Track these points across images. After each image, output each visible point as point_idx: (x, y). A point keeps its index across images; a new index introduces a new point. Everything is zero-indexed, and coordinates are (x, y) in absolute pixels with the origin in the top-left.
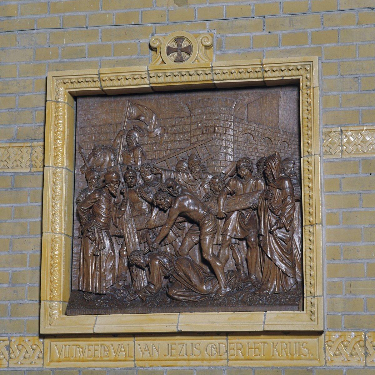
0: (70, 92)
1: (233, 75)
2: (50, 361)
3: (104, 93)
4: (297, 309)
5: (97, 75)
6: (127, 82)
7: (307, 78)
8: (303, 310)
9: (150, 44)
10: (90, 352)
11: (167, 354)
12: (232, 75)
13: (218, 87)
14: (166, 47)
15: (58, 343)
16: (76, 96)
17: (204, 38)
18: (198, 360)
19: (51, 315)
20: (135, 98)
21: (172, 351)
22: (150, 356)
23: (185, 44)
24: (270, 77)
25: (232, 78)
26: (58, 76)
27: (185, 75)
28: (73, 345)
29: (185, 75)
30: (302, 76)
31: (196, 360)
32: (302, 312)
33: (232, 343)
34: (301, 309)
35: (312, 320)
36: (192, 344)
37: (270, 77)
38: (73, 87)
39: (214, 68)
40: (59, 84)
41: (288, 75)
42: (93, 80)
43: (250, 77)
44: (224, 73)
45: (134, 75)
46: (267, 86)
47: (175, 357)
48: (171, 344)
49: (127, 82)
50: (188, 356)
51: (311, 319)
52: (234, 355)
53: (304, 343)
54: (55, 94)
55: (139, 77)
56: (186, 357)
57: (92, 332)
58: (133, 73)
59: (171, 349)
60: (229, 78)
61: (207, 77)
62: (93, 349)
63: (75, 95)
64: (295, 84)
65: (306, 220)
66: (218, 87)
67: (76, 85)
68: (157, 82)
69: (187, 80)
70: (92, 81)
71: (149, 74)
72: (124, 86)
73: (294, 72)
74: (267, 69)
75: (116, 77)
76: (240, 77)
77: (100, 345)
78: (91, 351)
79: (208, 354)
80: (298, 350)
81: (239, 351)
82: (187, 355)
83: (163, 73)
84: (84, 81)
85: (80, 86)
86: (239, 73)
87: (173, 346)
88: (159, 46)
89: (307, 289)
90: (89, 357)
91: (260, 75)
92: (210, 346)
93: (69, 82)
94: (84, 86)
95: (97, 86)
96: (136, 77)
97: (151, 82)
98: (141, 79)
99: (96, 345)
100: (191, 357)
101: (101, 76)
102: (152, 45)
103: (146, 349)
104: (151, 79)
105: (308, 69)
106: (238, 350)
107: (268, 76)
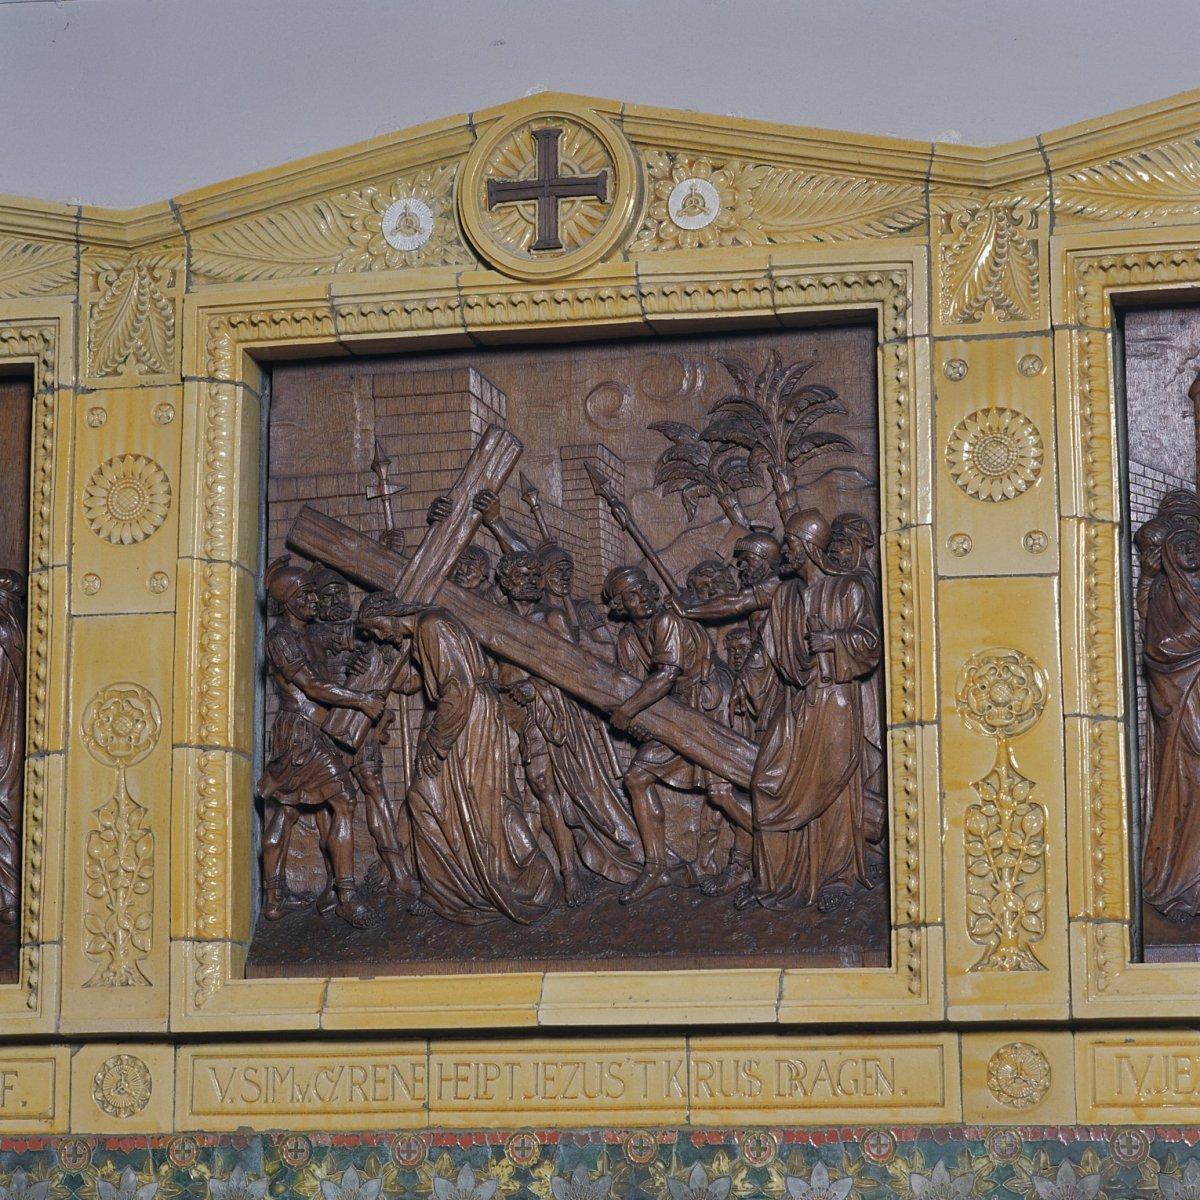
0: (249, 352)
2: (1094, 1106)
11: (533, 1093)
12: (665, 299)
13: (356, 352)
16: (269, 363)
22: (712, 1095)
24: (700, 311)
26: (852, 264)
28: (638, 1062)
30: (882, 301)
33: (383, 1066)
36: (737, 1062)
38: (256, 336)
39: (336, 302)
41: (855, 300)
44: (363, 314)
49: (801, 296)
54: (205, 358)
55: (591, 294)
56: (583, 1101)
57: (535, 1024)
58: (1147, 249)
64: (867, 320)
65: (895, 711)
69: (549, 317)
70: (794, 286)
71: (639, 286)
73: (859, 292)
74: (783, 283)
81: (357, 1089)
83: (310, 308)
84: (504, 300)
87: (551, 1070)
91: (766, 298)
98: (553, 303)
99: (11, 1072)
100: (596, 1102)
101: (642, 280)
103: (823, 1073)
105: (48, 336)
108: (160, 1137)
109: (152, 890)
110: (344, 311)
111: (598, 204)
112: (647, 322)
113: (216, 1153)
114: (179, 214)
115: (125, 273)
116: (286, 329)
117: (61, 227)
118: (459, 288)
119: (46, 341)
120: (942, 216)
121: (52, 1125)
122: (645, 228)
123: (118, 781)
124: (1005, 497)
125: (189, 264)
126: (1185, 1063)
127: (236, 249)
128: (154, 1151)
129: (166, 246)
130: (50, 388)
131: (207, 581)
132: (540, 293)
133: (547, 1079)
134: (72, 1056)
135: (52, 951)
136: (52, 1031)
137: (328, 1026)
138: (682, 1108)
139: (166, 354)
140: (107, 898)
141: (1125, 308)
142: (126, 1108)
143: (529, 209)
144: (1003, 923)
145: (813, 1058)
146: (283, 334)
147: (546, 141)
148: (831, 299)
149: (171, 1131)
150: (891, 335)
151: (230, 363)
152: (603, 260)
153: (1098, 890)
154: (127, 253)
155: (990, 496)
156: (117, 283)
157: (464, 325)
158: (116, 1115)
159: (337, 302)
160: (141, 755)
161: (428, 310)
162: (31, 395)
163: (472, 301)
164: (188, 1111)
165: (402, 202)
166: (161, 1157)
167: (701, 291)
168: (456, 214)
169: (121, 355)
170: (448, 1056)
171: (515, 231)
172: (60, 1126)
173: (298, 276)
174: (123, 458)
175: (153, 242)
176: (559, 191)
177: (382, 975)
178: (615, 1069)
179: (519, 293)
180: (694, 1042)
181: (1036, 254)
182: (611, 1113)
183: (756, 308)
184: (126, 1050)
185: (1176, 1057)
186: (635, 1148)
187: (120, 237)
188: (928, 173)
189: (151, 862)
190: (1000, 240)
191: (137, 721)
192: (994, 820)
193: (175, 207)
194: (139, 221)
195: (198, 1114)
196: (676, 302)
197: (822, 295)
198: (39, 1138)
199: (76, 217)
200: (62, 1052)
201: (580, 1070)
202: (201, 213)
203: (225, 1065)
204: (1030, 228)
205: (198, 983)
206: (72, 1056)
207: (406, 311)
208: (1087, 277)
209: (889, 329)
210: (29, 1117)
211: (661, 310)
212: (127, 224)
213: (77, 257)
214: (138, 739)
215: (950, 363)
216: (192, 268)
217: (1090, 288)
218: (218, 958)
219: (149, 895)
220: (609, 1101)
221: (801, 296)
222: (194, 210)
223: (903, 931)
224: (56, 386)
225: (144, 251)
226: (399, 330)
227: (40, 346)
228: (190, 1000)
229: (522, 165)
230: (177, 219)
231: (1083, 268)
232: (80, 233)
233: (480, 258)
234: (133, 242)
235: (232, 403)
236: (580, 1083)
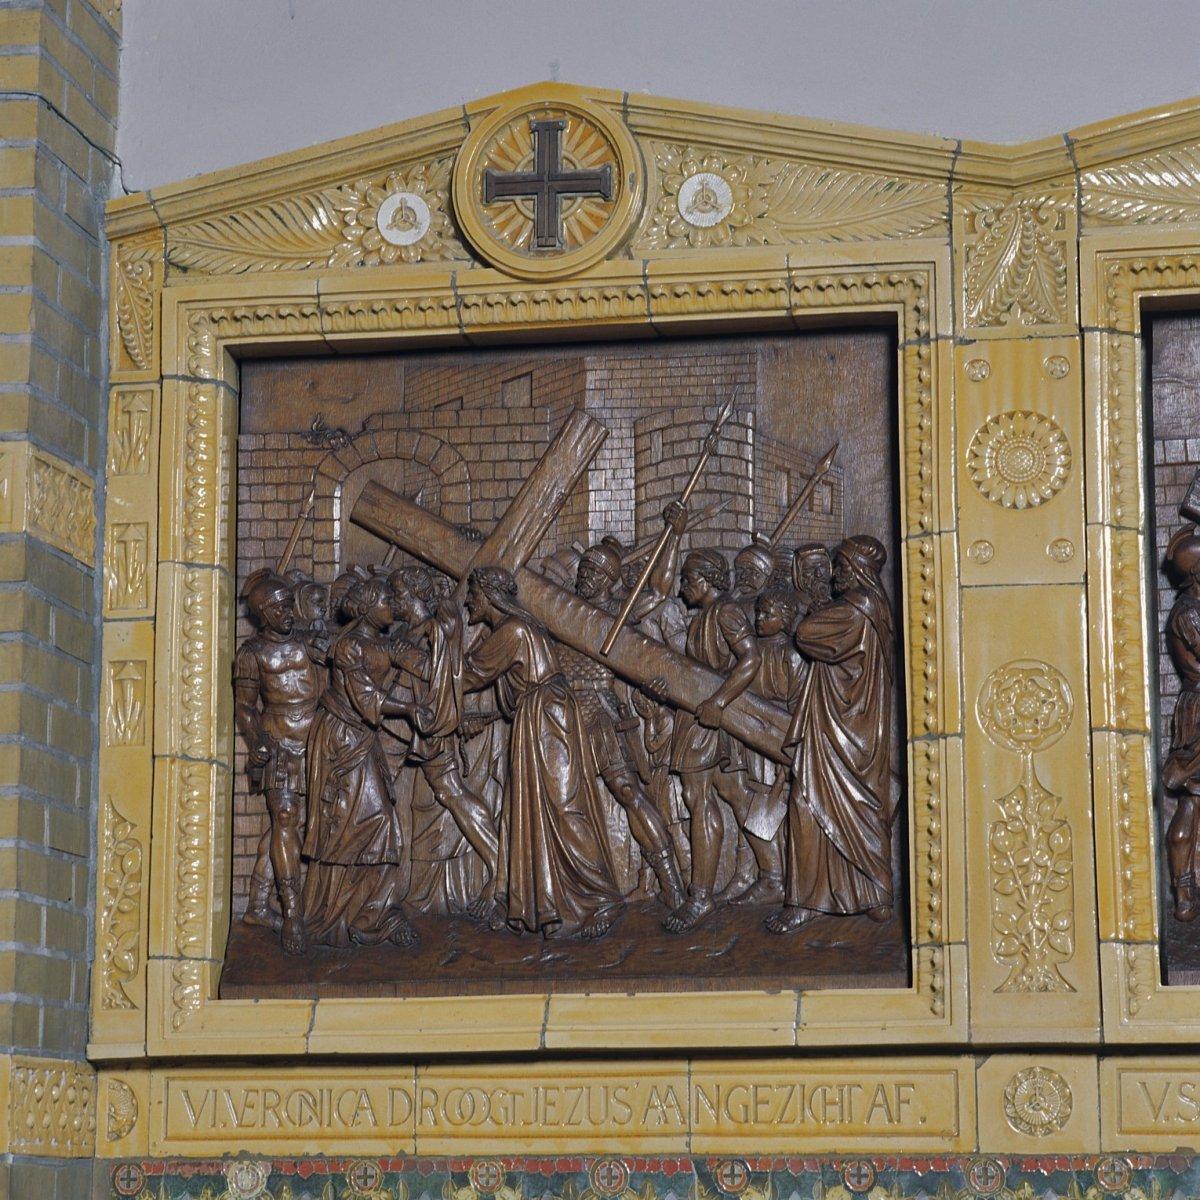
0: (227, 348)
5: (313, 296)
7: (917, 309)
8: (910, 985)
10: (906, 1105)
11: (532, 1119)
15: (233, 1085)
16: (244, 358)
21: (828, 1107)
24: (435, 327)
25: (376, 326)
30: (903, 302)
32: (907, 991)
34: (904, 981)
35: (934, 1012)
37: (411, 328)
39: (460, 292)
40: (197, 324)
42: (277, 311)
47: (553, 1128)
48: (546, 1089)
55: (737, 287)
62: (261, 1101)
64: (884, 326)
70: (274, 316)
73: (881, 293)
74: (658, 291)
75: (414, 303)
78: (908, 1102)
79: (815, 1118)
85: (725, 306)
89: (921, 923)
91: (783, 299)
92: (296, 1097)
94: (275, 329)
95: (312, 329)
96: (752, 286)
100: (603, 1128)
101: (322, 298)
104: (653, 301)
105: (920, 281)
108: (1085, 1157)
109: (1071, 887)
110: (331, 309)
111: (601, 201)
112: (793, 318)
113: (1152, 1176)
114: (1072, 150)
115: (1006, 214)
117: (933, 163)
119: (917, 286)
120: (966, 216)
121: (957, 1143)
122: (655, 224)
123: (1025, 767)
124: (1030, 505)
125: (1079, 206)
126: (906, 1092)
127: (204, 238)
128: (1079, 1173)
129: (1053, 185)
130: (924, 339)
132: (541, 292)
133: (900, 1102)
134: (977, 1068)
135: (958, 951)
136: (964, 1039)
137: (804, 1042)
138: (681, 1135)
139: (1057, 303)
140: (1017, 897)
141: (1155, 314)
142: (1042, 1125)
143: (526, 206)
144: (1030, 942)
145: (338, 1085)
146: (1189, 282)
147: (547, 133)
148: (827, 302)
149: (1097, 1152)
151: (211, 363)
152: (609, 257)
153: (1129, 912)
154: (1008, 192)
155: (1000, 500)
156: (997, 224)
157: (459, 326)
158: (1031, 1134)
160: (1052, 738)
163: (469, 301)
164: (163, 1136)
165: (398, 197)
166: (1089, 1180)
168: (451, 210)
169: (1003, 304)
170: (888, 1077)
171: (513, 226)
172: (966, 1145)
173: (289, 269)
174: (1011, 416)
175: (1039, 180)
176: (557, 185)
177: (328, 997)
178: (621, 1093)
179: (519, 292)
180: (422, 1070)
181: (1064, 256)
182: (495, 1142)
183: (843, 305)
184: (1040, 1062)
185: (898, 1086)
186: (853, 1175)
187: (1004, 175)
188: (951, 172)
189: (1069, 854)
190: (1026, 241)
191: (1044, 702)
192: (1020, 838)
193: (1070, 143)
194: (1027, 157)
195: (1128, 1132)
197: (393, 319)
198: (940, 1159)
199: (953, 152)
200: (967, 1062)
201: (584, 1099)
202: (1099, 149)
203: (1156, 1080)
204: (1057, 228)
205: (175, 1003)
206: (977, 1068)
208: (1117, 280)
210: (931, 1134)
211: (668, 312)
212: (1013, 160)
213: (949, 196)
214: (1047, 723)
215: (1051, 359)
216: (1083, 209)
217: (1120, 291)
219: (1069, 890)
220: (616, 1127)
221: (820, 298)
222: (1090, 146)
223: (925, 951)
224: (932, 336)
225: (1028, 190)
226: (364, 331)
227: (906, 292)
228: (168, 1020)
229: (520, 157)
230: (1071, 155)
231: (1114, 269)
232: (957, 168)
233: (476, 256)
234: (1017, 180)
235: (213, 404)
236: (585, 1107)
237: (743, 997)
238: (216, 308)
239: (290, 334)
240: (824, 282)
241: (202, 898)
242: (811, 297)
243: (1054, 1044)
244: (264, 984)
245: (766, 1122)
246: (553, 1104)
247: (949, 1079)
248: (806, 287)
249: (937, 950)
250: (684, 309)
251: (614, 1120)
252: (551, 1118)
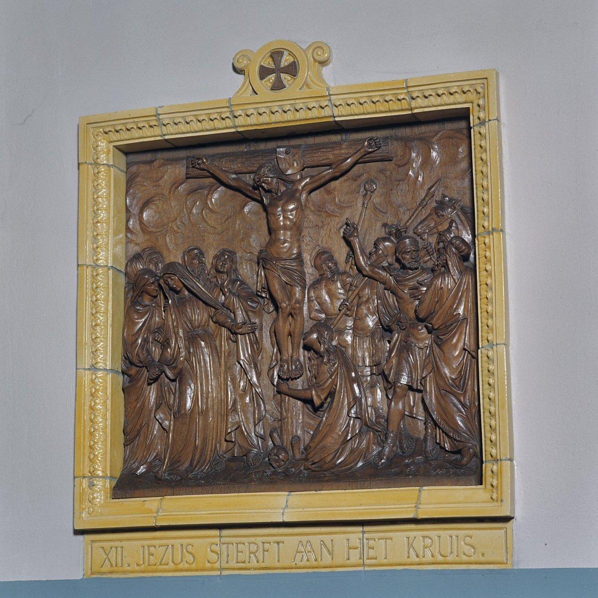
0: (117, 148)
1: (363, 107)
3: (168, 145)
4: (302, 489)
6: (439, 100)
7: (479, 106)
9: (235, 65)
12: (386, 103)
13: (247, 136)
14: (257, 69)
17: (316, 50)
18: (484, 564)
19: (91, 499)
20: (366, 134)
23: (286, 60)
24: (381, 112)
27: (288, 110)
29: (290, 110)
30: (472, 102)
31: (313, 568)
32: (480, 486)
33: (267, 543)
35: (493, 499)
37: (381, 112)
39: (410, 89)
40: (97, 135)
42: (220, 116)
43: (391, 109)
44: (348, 105)
45: (436, 88)
46: (420, 121)
49: (439, 100)
50: (444, 556)
51: (491, 498)
52: (244, 562)
53: (188, 545)
59: (238, 552)
60: (356, 111)
61: (324, 113)
63: (126, 151)
64: (463, 115)
66: (345, 128)
67: (125, 135)
68: (321, 116)
69: (304, 117)
70: (171, 123)
71: (330, 100)
72: (369, 113)
73: (459, 98)
76: (201, 129)
77: (148, 546)
80: (456, 547)
81: (252, 555)
82: (465, 555)
84: (317, 106)
86: (372, 104)
88: (247, 66)
90: (239, 563)
93: (113, 130)
94: (126, 137)
95: (156, 134)
97: (237, 124)
98: (436, 96)
100: (180, 566)
102: (237, 66)
104: (236, 119)
105: (480, 90)
106: (426, 548)
107: (417, 105)
116: (136, 133)
118: (407, 87)
131: (94, 277)
150: (477, 121)
157: (411, 109)
159: (161, 117)
161: (211, 120)
162: (469, 128)
167: (255, 114)
185: (149, 546)
196: (447, 99)
205: (90, 501)
207: (373, 102)
209: (476, 118)
218: (103, 487)
220: (187, 566)
227: (472, 96)
237: (242, 496)
238: (387, 95)
239: (145, 138)
240: (440, 92)
241: (104, 445)
242: (420, 102)
243: (237, 523)
244: (189, 486)
245: (242, 562)
246: (153, 555)
247: (503, 531)
248: (444, 94)
249: (495, 463)
250: (145, 135)
251: (187, 563)
252: (239, 559)
